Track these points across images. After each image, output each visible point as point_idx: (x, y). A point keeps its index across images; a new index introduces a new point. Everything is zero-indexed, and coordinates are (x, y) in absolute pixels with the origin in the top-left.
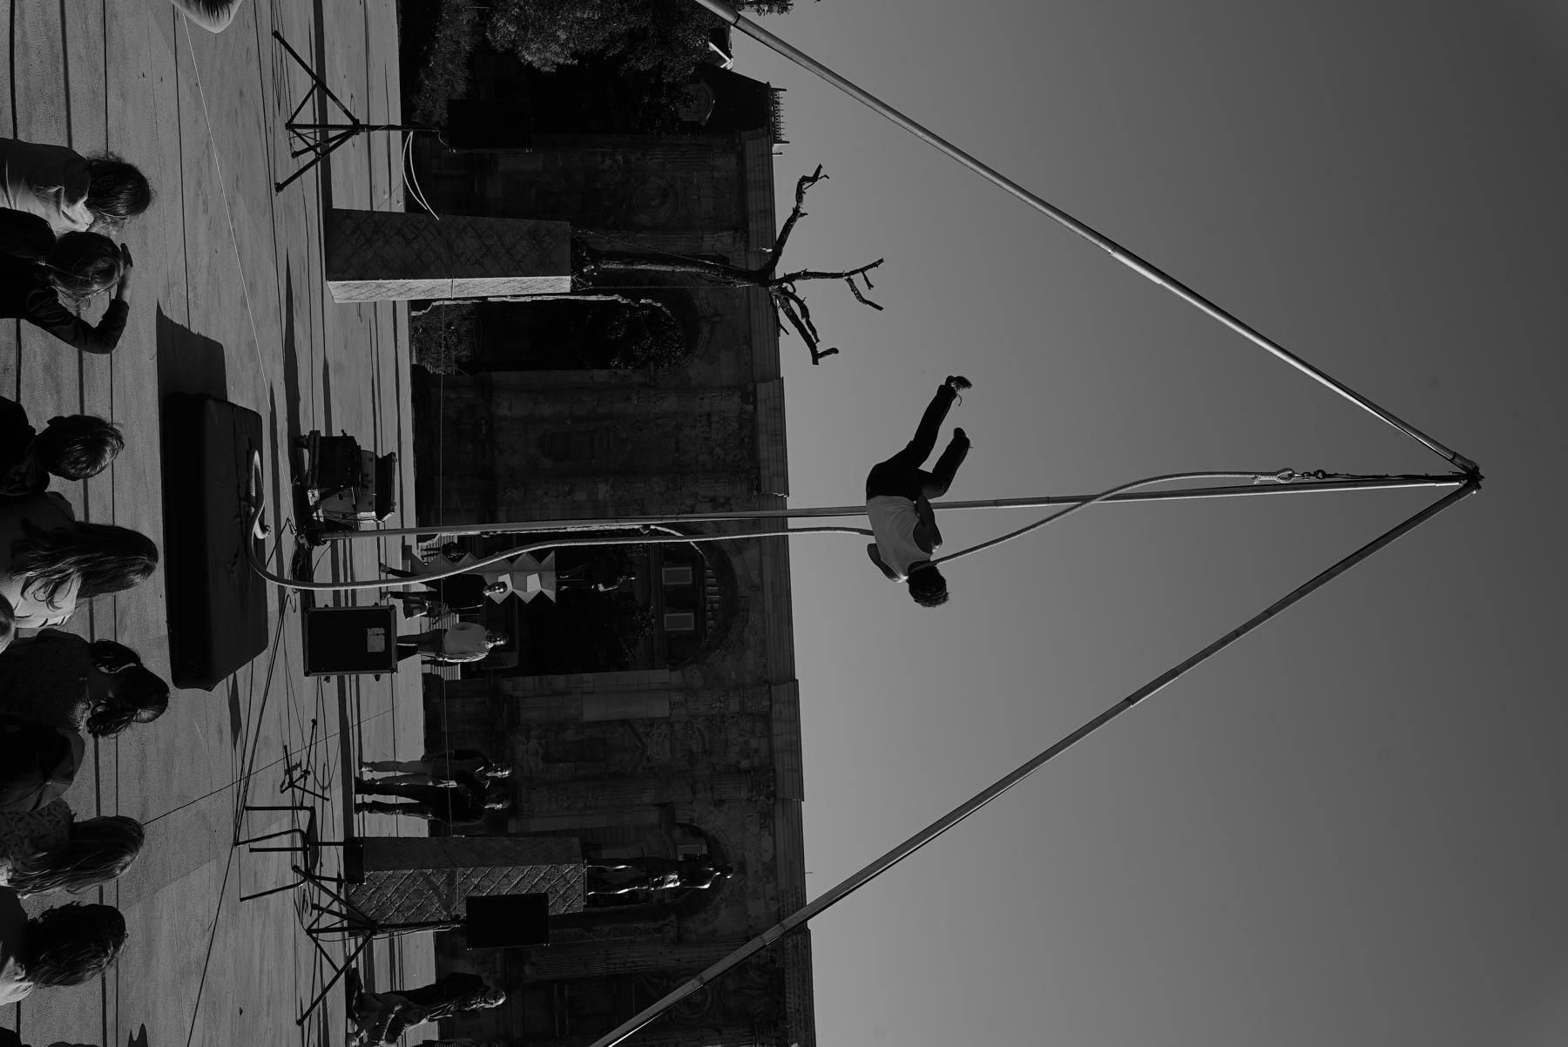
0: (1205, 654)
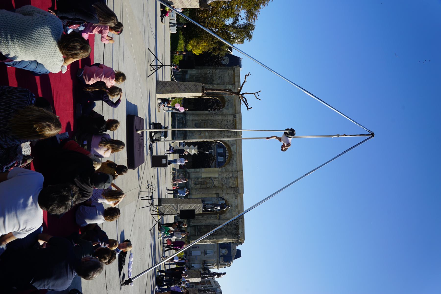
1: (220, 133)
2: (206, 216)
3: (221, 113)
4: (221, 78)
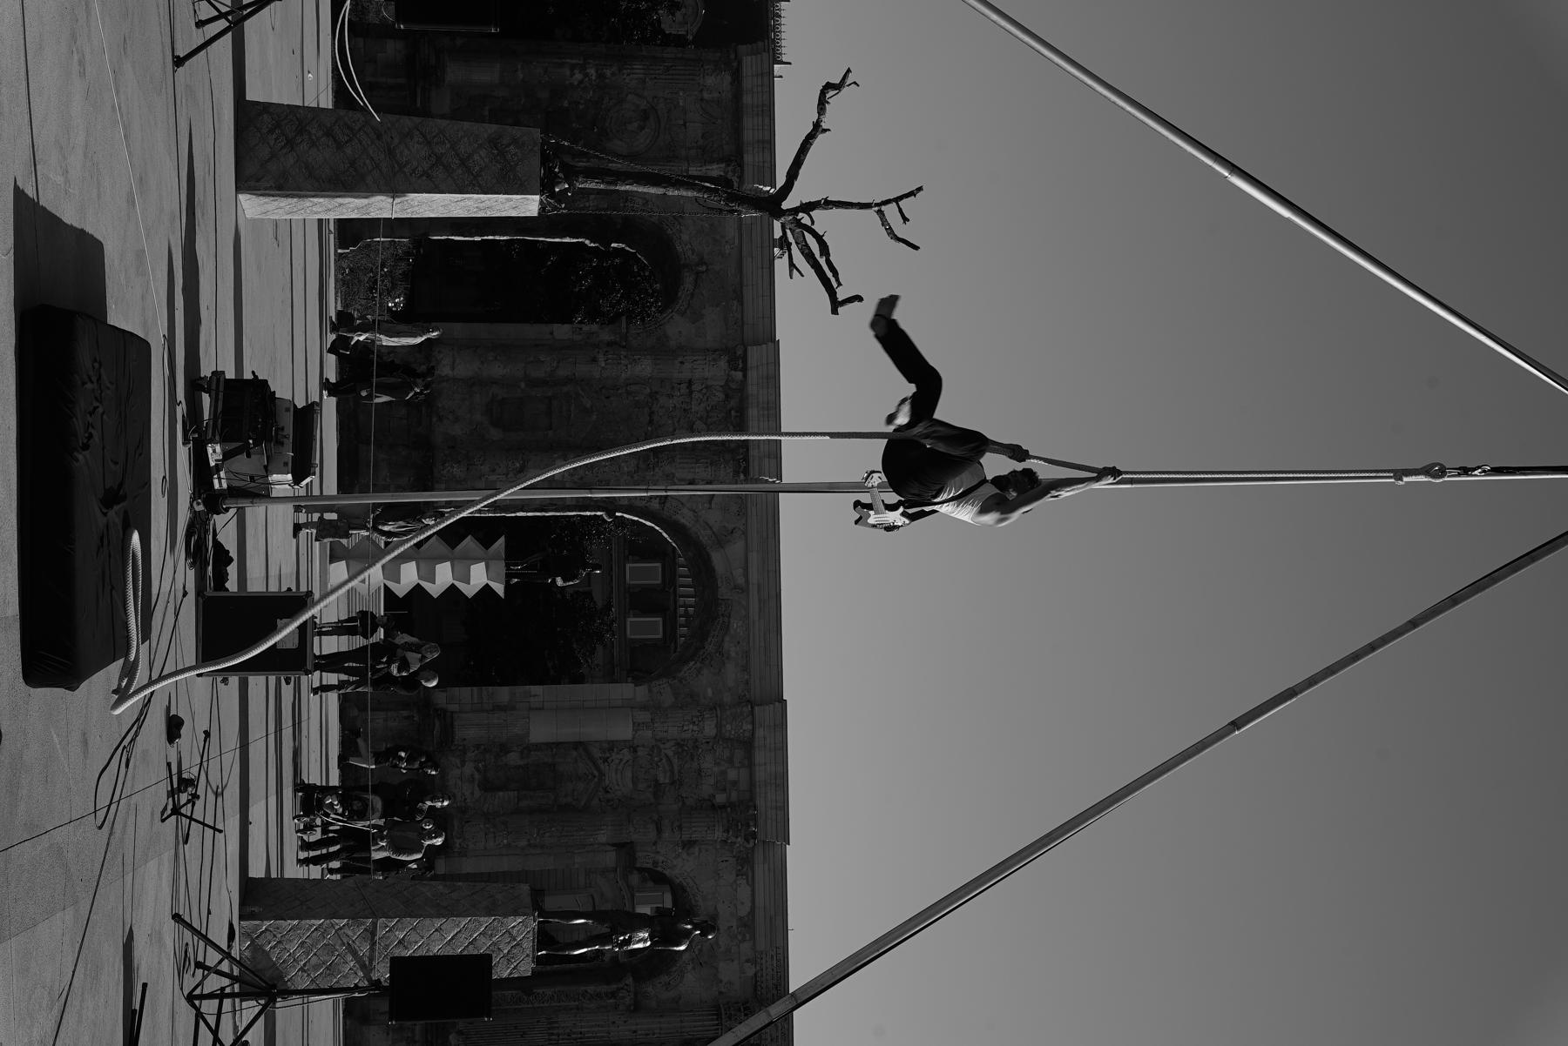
0: (1331, 671)
2: (549, 992)
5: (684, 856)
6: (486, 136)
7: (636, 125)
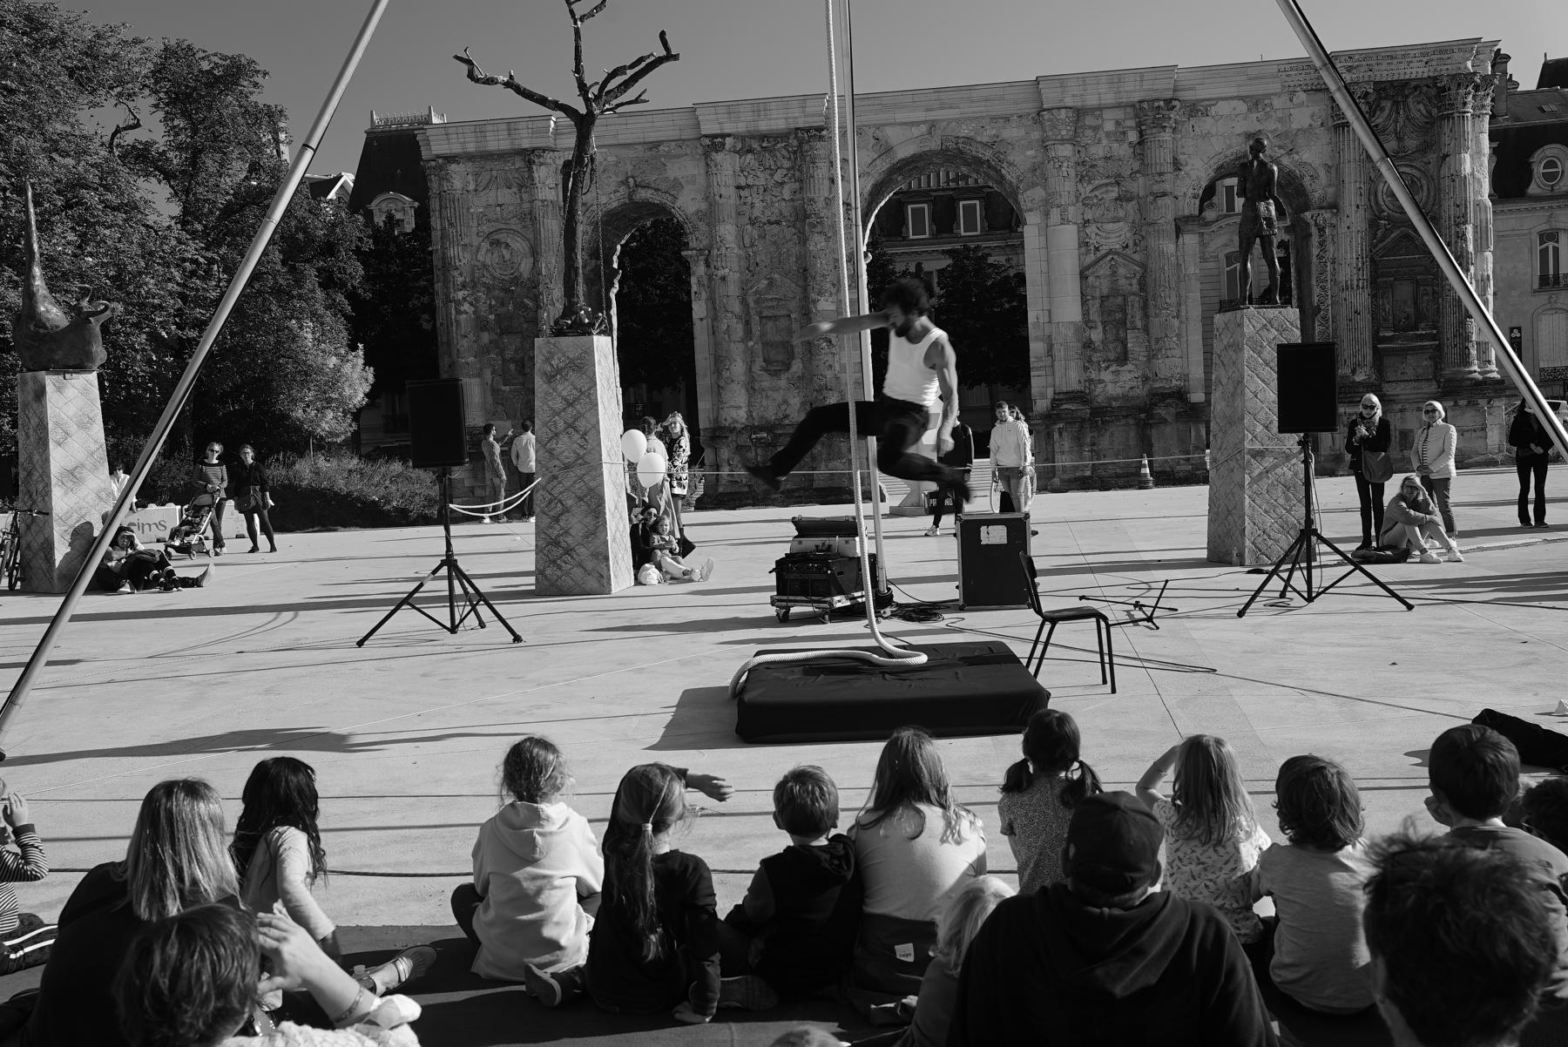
1: (819, 229)
2: (1317, 291)
3: (702, 226)
4: (501, 237)
5: (1188, 168)
6: (545, 386)
7: (505, 252)
